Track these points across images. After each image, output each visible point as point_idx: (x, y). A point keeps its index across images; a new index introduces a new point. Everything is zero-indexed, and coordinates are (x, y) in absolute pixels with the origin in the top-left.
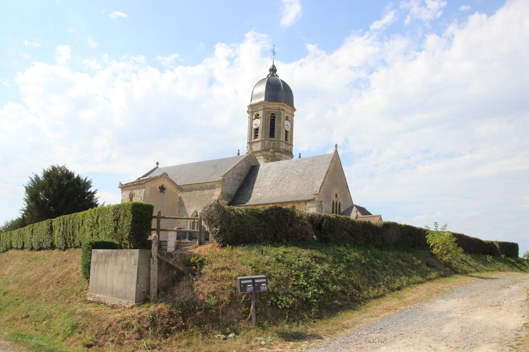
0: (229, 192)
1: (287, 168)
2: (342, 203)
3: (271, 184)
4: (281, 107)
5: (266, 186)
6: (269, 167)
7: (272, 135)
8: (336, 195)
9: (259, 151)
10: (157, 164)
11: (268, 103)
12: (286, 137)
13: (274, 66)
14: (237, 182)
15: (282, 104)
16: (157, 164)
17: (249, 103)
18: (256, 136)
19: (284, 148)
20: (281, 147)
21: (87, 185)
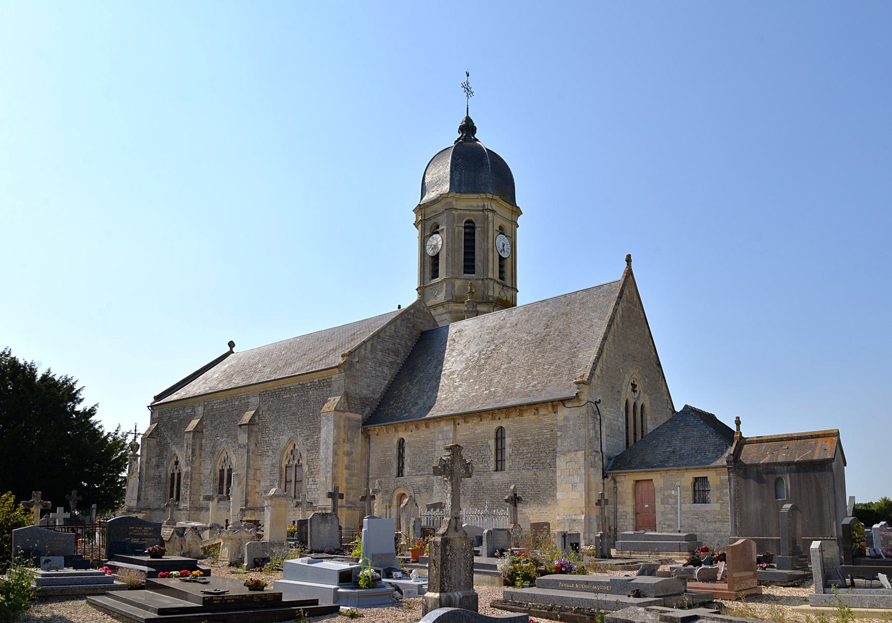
0: (365, 392)
1: (501, 328)
2: (647, 406)
3: (465, 369)
4: (488, 205)
5: (453, 373)
6: (460, 331)
7: (469, 267)
8: (634, 386)
9: (442, 305)
10: (231, 344)
11: (458, 195)
12: (501, 273)
13: (468, 120)
14: (386, 369)
15: (490, 196)
16: (231, 344)
17: (416, 202)
18: (435, 274)
19: (497, 295)
20: (491, 293)
21: (59, 393)
